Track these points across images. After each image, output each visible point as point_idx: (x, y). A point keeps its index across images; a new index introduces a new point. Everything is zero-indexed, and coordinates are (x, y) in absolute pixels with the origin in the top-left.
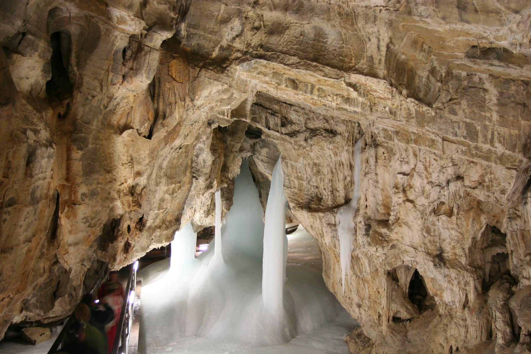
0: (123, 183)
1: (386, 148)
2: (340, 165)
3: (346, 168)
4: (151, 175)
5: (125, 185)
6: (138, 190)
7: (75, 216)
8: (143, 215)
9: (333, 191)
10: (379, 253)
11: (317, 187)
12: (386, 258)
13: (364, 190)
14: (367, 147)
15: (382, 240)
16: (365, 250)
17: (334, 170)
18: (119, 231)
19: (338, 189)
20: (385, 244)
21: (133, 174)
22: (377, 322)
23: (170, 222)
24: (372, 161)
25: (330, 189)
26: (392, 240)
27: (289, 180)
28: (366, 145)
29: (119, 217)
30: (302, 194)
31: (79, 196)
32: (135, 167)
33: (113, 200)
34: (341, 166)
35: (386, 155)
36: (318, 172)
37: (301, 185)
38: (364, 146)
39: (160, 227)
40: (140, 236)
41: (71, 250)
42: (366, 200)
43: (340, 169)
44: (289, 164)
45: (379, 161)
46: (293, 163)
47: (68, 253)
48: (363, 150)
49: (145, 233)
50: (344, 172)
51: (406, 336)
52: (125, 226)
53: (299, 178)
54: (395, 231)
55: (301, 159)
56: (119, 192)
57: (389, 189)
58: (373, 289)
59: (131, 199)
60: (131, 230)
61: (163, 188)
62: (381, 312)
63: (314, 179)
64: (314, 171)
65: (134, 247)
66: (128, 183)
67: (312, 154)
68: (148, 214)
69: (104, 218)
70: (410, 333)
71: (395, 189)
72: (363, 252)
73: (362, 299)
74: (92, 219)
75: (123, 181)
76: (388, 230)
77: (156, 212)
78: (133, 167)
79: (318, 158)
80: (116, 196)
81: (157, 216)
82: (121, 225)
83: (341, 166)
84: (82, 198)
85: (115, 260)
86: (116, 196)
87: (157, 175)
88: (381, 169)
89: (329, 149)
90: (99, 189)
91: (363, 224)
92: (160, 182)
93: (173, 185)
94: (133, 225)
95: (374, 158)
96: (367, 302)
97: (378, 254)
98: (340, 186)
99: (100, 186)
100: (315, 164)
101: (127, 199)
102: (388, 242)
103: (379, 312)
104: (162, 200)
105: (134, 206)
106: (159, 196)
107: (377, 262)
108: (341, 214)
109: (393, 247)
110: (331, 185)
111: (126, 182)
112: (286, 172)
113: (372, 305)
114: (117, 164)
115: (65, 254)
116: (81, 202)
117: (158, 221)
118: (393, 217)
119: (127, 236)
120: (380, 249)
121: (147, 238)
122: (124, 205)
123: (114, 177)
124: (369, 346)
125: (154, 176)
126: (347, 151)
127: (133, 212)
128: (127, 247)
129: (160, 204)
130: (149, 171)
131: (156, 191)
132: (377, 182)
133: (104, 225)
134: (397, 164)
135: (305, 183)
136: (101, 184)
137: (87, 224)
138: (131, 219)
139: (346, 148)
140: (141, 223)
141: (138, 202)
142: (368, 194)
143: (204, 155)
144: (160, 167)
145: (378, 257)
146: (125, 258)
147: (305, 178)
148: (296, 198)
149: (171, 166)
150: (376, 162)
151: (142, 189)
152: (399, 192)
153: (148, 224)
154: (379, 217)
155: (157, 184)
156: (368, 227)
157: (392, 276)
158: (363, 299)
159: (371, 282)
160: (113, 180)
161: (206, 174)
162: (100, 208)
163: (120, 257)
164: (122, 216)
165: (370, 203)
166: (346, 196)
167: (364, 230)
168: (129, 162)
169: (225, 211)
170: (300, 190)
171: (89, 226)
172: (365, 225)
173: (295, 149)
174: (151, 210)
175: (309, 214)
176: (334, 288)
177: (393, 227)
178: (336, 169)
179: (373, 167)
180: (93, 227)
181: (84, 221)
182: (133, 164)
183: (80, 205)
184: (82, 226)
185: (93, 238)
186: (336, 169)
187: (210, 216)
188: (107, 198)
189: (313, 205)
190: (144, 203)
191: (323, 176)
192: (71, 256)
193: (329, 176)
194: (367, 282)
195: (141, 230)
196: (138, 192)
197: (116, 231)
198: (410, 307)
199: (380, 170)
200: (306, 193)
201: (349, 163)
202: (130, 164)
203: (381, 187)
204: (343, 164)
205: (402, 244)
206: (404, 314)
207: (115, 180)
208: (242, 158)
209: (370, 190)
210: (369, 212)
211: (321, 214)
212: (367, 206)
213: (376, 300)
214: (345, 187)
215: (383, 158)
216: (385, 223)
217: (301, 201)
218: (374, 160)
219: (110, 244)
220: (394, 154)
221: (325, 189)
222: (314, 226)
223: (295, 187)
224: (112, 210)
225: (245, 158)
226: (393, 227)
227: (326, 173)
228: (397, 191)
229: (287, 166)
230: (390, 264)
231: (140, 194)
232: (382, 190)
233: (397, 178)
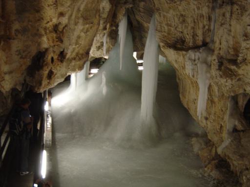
0: (49, 22)
1: (240, 6)
2: (201, 17)
3: (205, 19)
4: (71, 16)
5: (51, 23)
6: (61, 28)
7: (10, 48)
8: (64, 49)
9: (194, 35)
10: (227, 84)
11: (182, 32)
12: (232, 87)
13: (220, 37)
14: (225, 4)
15: (231, 74)
16: (217, 80)
17: (196, 20)
18: (44, 61)
19: (198, 35)
20: (234, 77)
21: (57, 14)
22: (219, 130)
23: (82, 55)
24: (228, 15)
25: (192, 34)
26: (239, 75)
27: (161, 26)
28: (223, 2)
29: (44, 50)
30: (170, 37)
31: (13, 32)
32: (59, 8)
33: (41, 36)
34: (202, 18)
35: (239, 11)
36: (184, 21)
37: (170, 30)
38: (221, 3)
39: (74, 59)
40: (61, 66)
41: (7, 77)
42: (220, 44)
43: (200, 20)
44: (162, 15)
45: (233, 15)
46: (165, 14)
47: (4, 80)
48: (221, 6)
49: (65, 64)
50: (203, 22)
51: (240, 142)
52: (50, 58)
53: (168, 25)
54: (242, 68)
55: (171, 11)
56: (45, 29)
57: (238, 37)
58: (218, 108)
59: (55, 35)
60: (54, 61)
61: (80, 27)
62: (223, 124)
63: (180, 27)
64: (181, 20)
65: (56, 74)
66: (53, 22)
67: (180, 8)
68: (68, 49)
69: (34, 51)
70: (242, 140)
71: (245, 38)
72: (215, 82)
73: (210, 114)
74: (24, 52)
75: (49, 20)
76: (236, 67)
77: (74, 46)
78: (57, 8)
79: (184, 10)
80: (43, 32)
81: (74, 49)
82: (46, 56)
83: (202, 18)
84: (15, 33)
85: (41, 84)
86: (43, 32)
87: (76, 17)
88: (234, 21)
89: (194, 4)
90: (30, 27)
91: (217, 61)
92: (78, 22)
93: (88, 25)
94: (55, 57)
95: (230, 12)
96: (213, 117)
97: (227, 84)
98: (200, 32)
99: (30, 23)
100: (182, 15)
101: (52, 36)
102: (235, 76)
103: (221, 124)
104: (79, 37)
105: (57, 41)
106: (76, 33)
107: (225, 90)
108: (200, 52)
109: (239, 80)
110: (192, 31)
111: (51, 21)
112: (159, 20)
113: (216, 119)
114: (43, 5)
115: (2, 81)
116: (15, 37)
117: (74, 54)
118: (241, 58)
119: (51, 66)
120: (229, 81)
121: (66, 68)
122: (49, 40)
123: (42, 16)
124: (210, 146)
125: (73, 17)
126: (208, 6)
127: (56, 46)
128: (51, 75)
129: (77, 40)
130: (70, 12)
131: (74, 29)
132: (230, 31)
133: (33, 57)
134: (247, 18)
135: (172, 29)
136: (31, 22)
137: (20, 56)
138: (54, 52)
139: (207, 4)
140: (62, 56)
141: (61, 38)
142: (223, 41)
143: (104, 4)
144: (79, 10)
145: (226, 86)
146: (49, 83)
147: (173, 26)
148: (165, 39)
149: (86, 10)
150: (231, 16)
151: (64, 28)
152: (247, 40)
153: (68, 56)
154: (229, 57)
155: (76, 24)
156: (221, 64)
157: (235, 99)
158: (210, 114)
159: (217, 103)
160: (41, 19)
161: (104, 18)
162: (30, 43)
163: (45, 82)
164: (47, 50)
165: (224, 47)
166: (203, 40)
167: (217, 66)
168: (54, 4)
169: (111, 46)
170: (169, 34)
171: (21, 58)
172: (219, 62)
173: (167, 3)
174: (70, 45)
175: (175, 51)
176: (188, 104)
177: (240, 65)
178: (197, 19)
179: (228, 20)
180: (24, 58)
181: (17, 53)
182: (57, 5)
183: (14, 39)
184: (16, 58)
185: (24, 67)
186: (197, 19)
187: (101, 50)
188: (36, 34)
189: (178, 45)
190: (65, 40)
191: (187, 25)
192: (7, 82)
193: (192, 25)
194: (215, 103)
195: (62, 61)
196: (60, 30)
197: (41, 61)
198: (244, 122)
199: (233, 23)
200: (174, 36)
201: (208, 16)
202: (55, 5)
203: (233, 35)
204: (203, 16)
205: (247, 78)
206: (240, 127)
207: (42, 19)
208: (126, 8)
209: (224, 37)
210: (222, 53)
211: (184, 52)
212: (220, 49)
213: (220, 116)
214: (203, 34)
215: (237, 13)
216: (234, 62)
217: (169, 42)
218: (230, 14)
219: (37, 72)
220: (246, 11)
221: (188, 34)
222: (178, 61)
223: (165, 32)
224: (39, 44)
225: (128, 9)
226: (240, 65)
227: (190, 22)
228: (246, 39)
229: (160, 16)
230: (234, 91)
231: (62, 32)
232: (234, 37)
233: (246, 29)
